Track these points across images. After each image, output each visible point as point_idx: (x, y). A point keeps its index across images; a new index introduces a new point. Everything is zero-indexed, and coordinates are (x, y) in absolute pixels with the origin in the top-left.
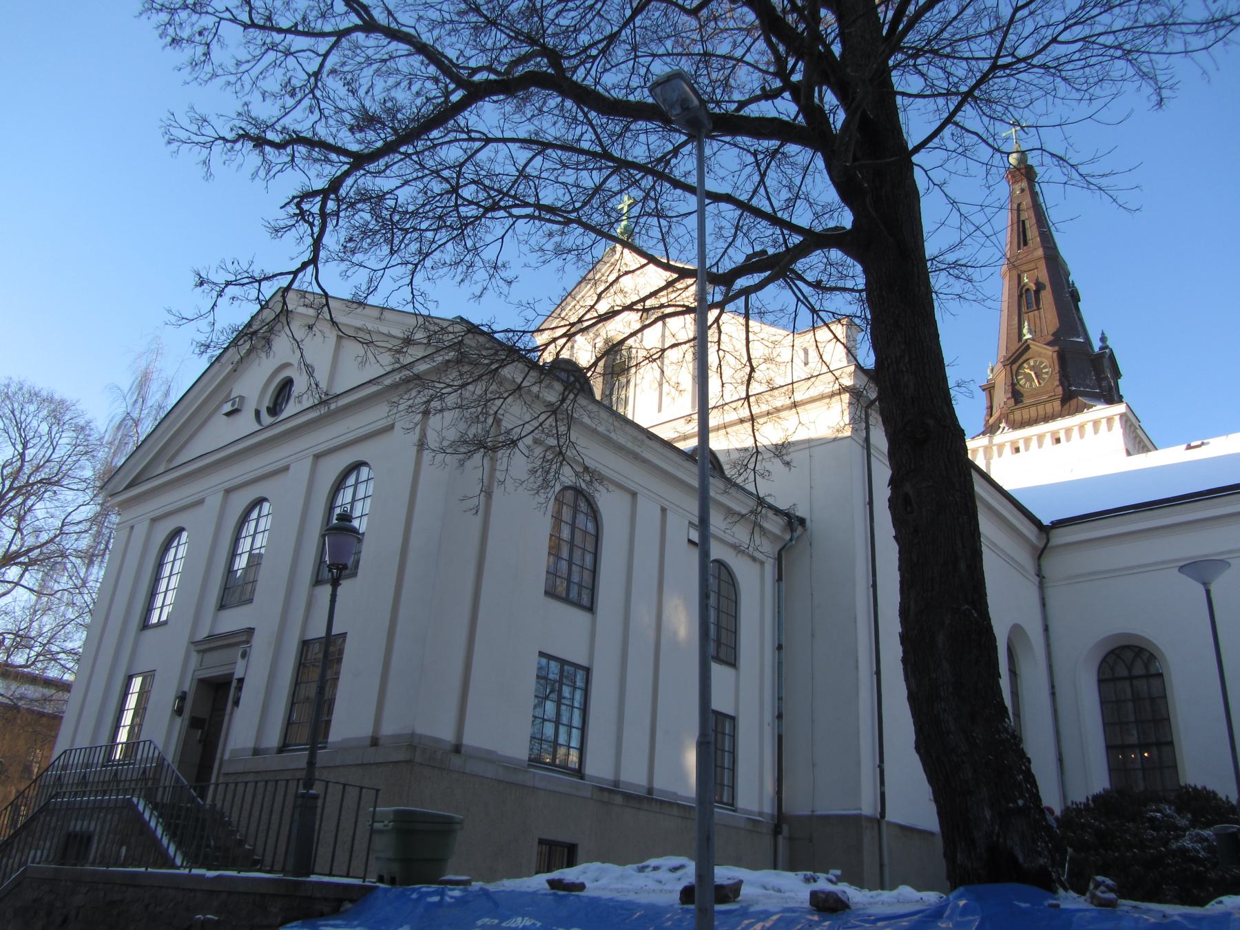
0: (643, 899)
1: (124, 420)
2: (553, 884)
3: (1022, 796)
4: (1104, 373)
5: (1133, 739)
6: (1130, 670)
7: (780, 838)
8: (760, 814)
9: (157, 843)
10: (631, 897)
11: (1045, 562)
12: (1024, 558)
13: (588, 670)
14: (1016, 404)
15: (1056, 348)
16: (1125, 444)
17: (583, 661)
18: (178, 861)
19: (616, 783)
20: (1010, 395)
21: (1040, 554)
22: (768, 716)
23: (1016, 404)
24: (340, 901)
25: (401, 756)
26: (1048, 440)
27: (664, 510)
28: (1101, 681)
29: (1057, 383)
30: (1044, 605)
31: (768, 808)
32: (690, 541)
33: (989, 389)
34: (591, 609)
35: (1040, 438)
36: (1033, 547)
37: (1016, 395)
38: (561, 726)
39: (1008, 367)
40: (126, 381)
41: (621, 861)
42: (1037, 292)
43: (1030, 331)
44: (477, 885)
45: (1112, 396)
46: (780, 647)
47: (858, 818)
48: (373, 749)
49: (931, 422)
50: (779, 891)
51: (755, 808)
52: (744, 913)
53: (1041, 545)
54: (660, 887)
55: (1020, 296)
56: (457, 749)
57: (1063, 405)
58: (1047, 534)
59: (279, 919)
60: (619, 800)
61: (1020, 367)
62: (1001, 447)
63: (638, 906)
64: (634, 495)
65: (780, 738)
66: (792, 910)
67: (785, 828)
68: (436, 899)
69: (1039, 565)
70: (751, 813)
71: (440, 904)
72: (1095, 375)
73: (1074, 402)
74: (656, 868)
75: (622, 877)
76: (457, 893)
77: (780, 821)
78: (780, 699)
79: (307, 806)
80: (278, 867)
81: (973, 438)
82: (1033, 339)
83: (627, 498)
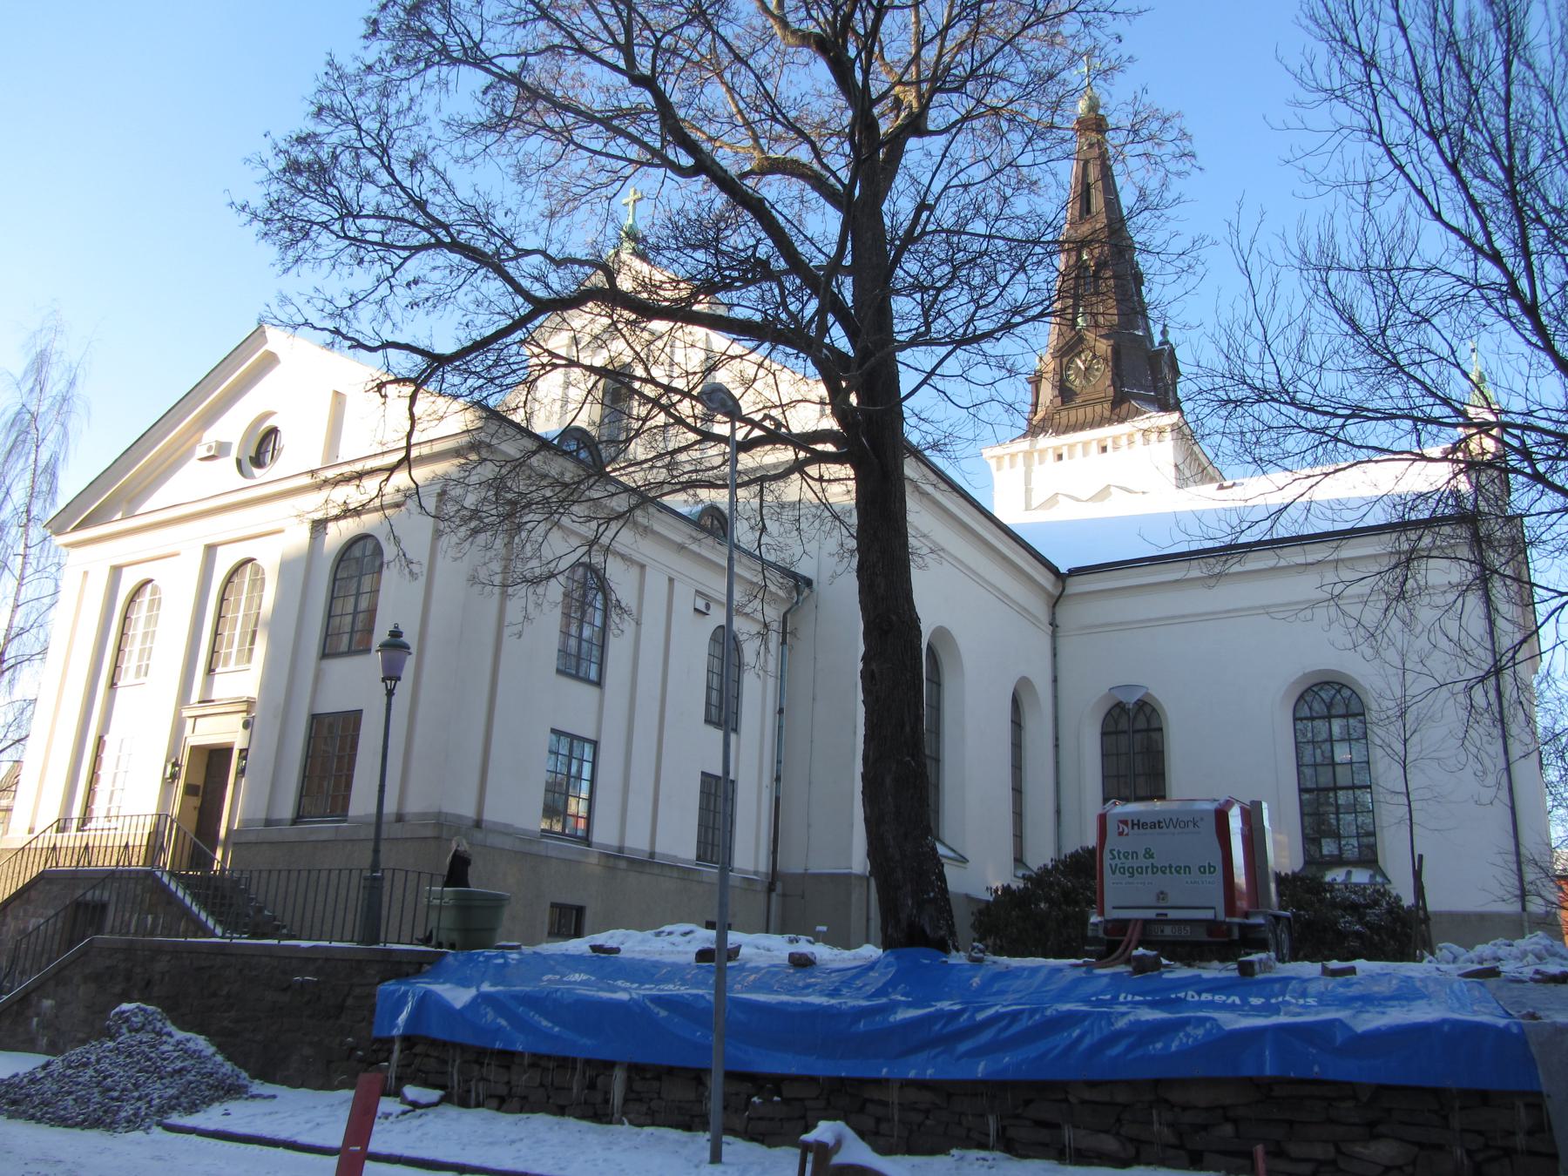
0: (668, 959)
1: (19, 413)
2: (595, 948)
3: (933, 890)
4: (1161, 372)
7: (774, 895)
8: (756, 873)
9: (186, 911)
10: (657, 957)
11: (1060, 610)
12: (1040, 609)
13: (595, 744)
15: (1112, 342)
16: (1175, 458)
17: (592, 736)
18: (219, 931)
19: (621, 849)
20: (1056, 392)
21: (1055, 602)
22: (767, 779)
24: (421, 964)
25: (429, 833)
26: (1094, 448)
27: (671, 580)
28: (1104, 734)
29: (1108, 382)
30: (1055, 655)
31: (763, 866)
32: (696, 610)
33: (1036, 380)
34: (599, 683)
35: (1086, 445)
36: (1050, 595)
37: (1065, 393)
38: (585, 815)
39: (1058, 360)
40: (19, 365)
41: (641, 928)
44: (527, 949)
45: (1168, 403)
46: (781, 711)
47: (848, 876)
48: (399, 825)
49: (894, 618)
50: (769, 950)
51: (750, 867)
52: (742, 968)
53: (1056, 593)
54: (674, 948)
56: (478, 824)
57: (1113, 409)
58: (1064, 582)
59: (377, 979)
60: (623, 864)
61: (1071, 361)
62: (1042, 452)
63: (665, 965)
64: (643, 567)
65: (777, 799)
66: (775, 966)
67: (779, 886)
68: (501, 961)
69: (1054, 614)
70: (746, 872)
71: (506, 964)
72: (1152, 373)
73: (1125, 407)
74: (670, 933)
75: (643, 941)
76: (515, 956)
77: (774, 878)
78: (779, 762)
79: (373, 886)
80: (348, 935)
83: (635, 571)
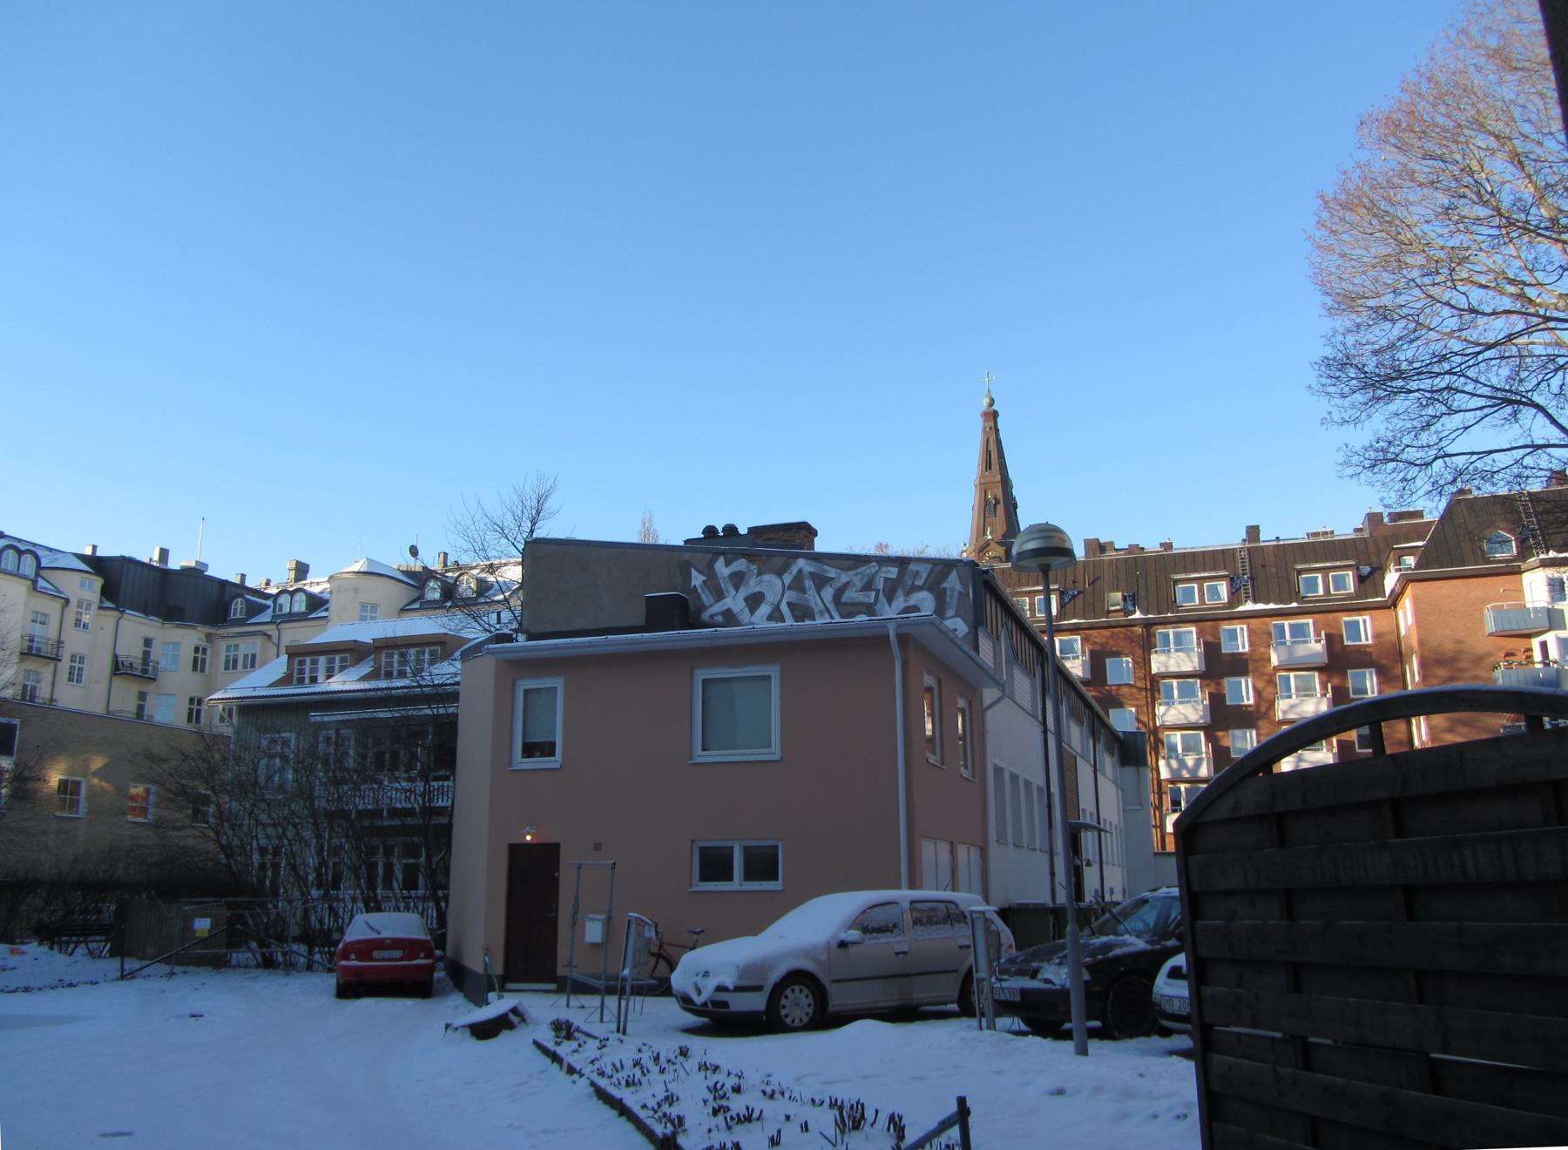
43: (991, 534)
55: (986, 505)
81: (956, 971)
82: (992, 540)
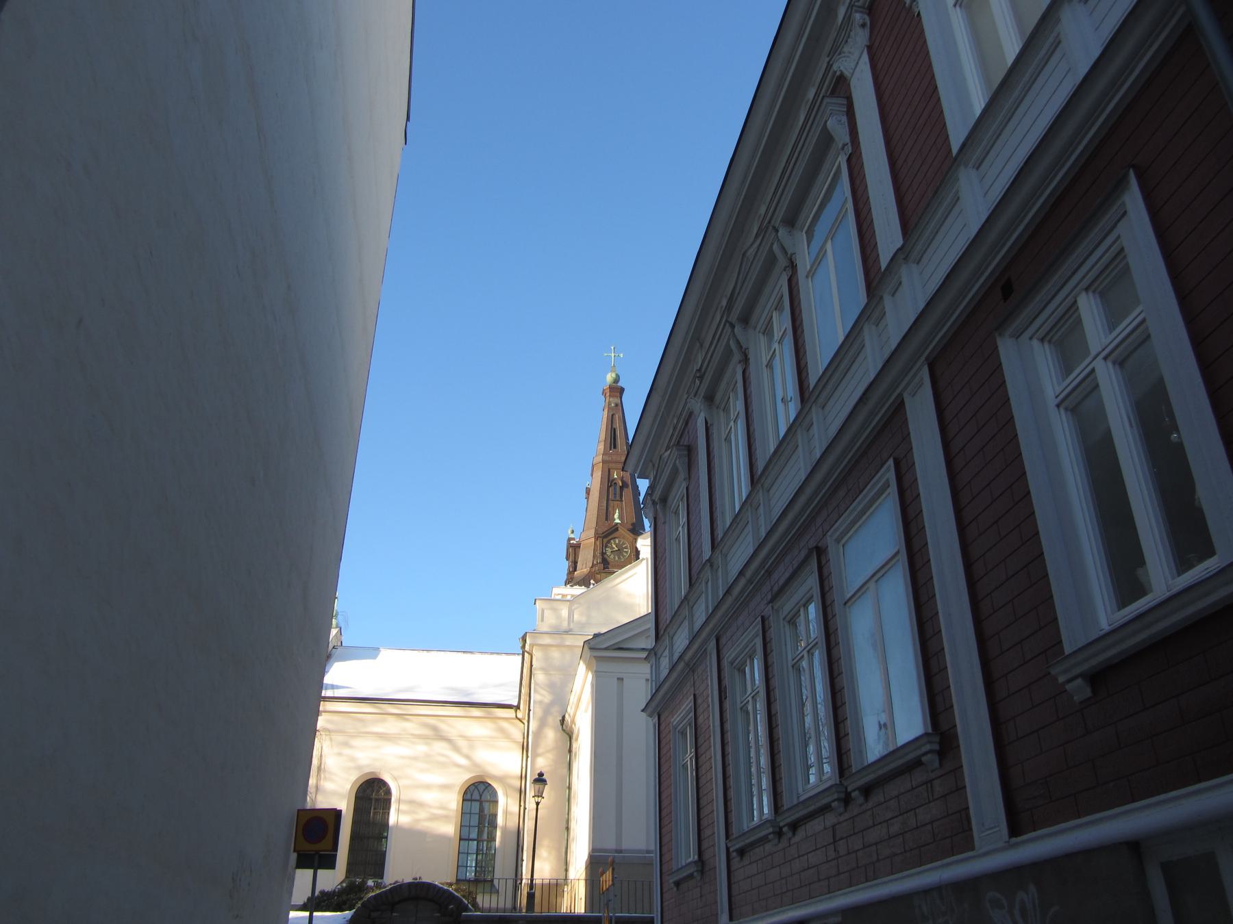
5: (478, 869)
6: (481, 796)
14: (604, 568)
23: (604, 568)
42: (621, 488)
61: (609, 542)
